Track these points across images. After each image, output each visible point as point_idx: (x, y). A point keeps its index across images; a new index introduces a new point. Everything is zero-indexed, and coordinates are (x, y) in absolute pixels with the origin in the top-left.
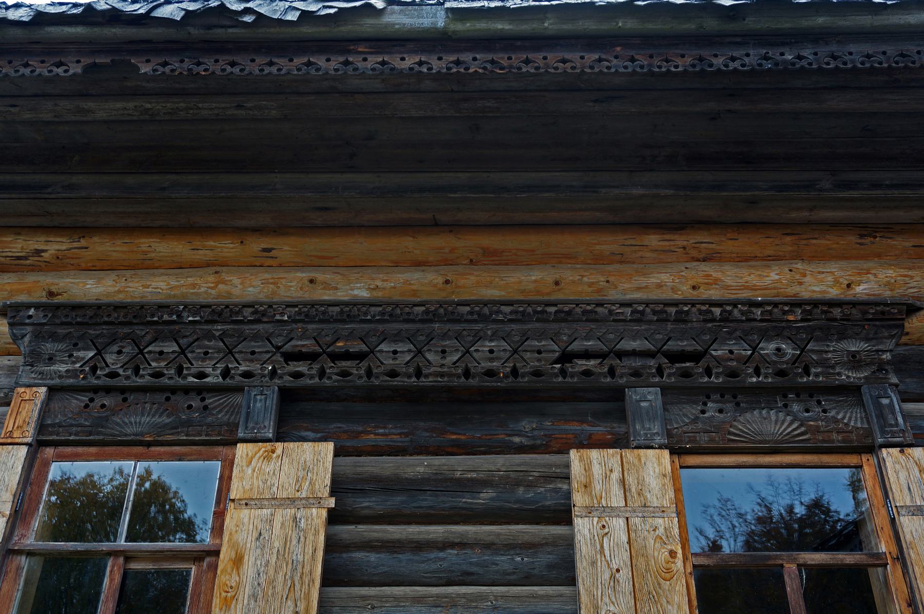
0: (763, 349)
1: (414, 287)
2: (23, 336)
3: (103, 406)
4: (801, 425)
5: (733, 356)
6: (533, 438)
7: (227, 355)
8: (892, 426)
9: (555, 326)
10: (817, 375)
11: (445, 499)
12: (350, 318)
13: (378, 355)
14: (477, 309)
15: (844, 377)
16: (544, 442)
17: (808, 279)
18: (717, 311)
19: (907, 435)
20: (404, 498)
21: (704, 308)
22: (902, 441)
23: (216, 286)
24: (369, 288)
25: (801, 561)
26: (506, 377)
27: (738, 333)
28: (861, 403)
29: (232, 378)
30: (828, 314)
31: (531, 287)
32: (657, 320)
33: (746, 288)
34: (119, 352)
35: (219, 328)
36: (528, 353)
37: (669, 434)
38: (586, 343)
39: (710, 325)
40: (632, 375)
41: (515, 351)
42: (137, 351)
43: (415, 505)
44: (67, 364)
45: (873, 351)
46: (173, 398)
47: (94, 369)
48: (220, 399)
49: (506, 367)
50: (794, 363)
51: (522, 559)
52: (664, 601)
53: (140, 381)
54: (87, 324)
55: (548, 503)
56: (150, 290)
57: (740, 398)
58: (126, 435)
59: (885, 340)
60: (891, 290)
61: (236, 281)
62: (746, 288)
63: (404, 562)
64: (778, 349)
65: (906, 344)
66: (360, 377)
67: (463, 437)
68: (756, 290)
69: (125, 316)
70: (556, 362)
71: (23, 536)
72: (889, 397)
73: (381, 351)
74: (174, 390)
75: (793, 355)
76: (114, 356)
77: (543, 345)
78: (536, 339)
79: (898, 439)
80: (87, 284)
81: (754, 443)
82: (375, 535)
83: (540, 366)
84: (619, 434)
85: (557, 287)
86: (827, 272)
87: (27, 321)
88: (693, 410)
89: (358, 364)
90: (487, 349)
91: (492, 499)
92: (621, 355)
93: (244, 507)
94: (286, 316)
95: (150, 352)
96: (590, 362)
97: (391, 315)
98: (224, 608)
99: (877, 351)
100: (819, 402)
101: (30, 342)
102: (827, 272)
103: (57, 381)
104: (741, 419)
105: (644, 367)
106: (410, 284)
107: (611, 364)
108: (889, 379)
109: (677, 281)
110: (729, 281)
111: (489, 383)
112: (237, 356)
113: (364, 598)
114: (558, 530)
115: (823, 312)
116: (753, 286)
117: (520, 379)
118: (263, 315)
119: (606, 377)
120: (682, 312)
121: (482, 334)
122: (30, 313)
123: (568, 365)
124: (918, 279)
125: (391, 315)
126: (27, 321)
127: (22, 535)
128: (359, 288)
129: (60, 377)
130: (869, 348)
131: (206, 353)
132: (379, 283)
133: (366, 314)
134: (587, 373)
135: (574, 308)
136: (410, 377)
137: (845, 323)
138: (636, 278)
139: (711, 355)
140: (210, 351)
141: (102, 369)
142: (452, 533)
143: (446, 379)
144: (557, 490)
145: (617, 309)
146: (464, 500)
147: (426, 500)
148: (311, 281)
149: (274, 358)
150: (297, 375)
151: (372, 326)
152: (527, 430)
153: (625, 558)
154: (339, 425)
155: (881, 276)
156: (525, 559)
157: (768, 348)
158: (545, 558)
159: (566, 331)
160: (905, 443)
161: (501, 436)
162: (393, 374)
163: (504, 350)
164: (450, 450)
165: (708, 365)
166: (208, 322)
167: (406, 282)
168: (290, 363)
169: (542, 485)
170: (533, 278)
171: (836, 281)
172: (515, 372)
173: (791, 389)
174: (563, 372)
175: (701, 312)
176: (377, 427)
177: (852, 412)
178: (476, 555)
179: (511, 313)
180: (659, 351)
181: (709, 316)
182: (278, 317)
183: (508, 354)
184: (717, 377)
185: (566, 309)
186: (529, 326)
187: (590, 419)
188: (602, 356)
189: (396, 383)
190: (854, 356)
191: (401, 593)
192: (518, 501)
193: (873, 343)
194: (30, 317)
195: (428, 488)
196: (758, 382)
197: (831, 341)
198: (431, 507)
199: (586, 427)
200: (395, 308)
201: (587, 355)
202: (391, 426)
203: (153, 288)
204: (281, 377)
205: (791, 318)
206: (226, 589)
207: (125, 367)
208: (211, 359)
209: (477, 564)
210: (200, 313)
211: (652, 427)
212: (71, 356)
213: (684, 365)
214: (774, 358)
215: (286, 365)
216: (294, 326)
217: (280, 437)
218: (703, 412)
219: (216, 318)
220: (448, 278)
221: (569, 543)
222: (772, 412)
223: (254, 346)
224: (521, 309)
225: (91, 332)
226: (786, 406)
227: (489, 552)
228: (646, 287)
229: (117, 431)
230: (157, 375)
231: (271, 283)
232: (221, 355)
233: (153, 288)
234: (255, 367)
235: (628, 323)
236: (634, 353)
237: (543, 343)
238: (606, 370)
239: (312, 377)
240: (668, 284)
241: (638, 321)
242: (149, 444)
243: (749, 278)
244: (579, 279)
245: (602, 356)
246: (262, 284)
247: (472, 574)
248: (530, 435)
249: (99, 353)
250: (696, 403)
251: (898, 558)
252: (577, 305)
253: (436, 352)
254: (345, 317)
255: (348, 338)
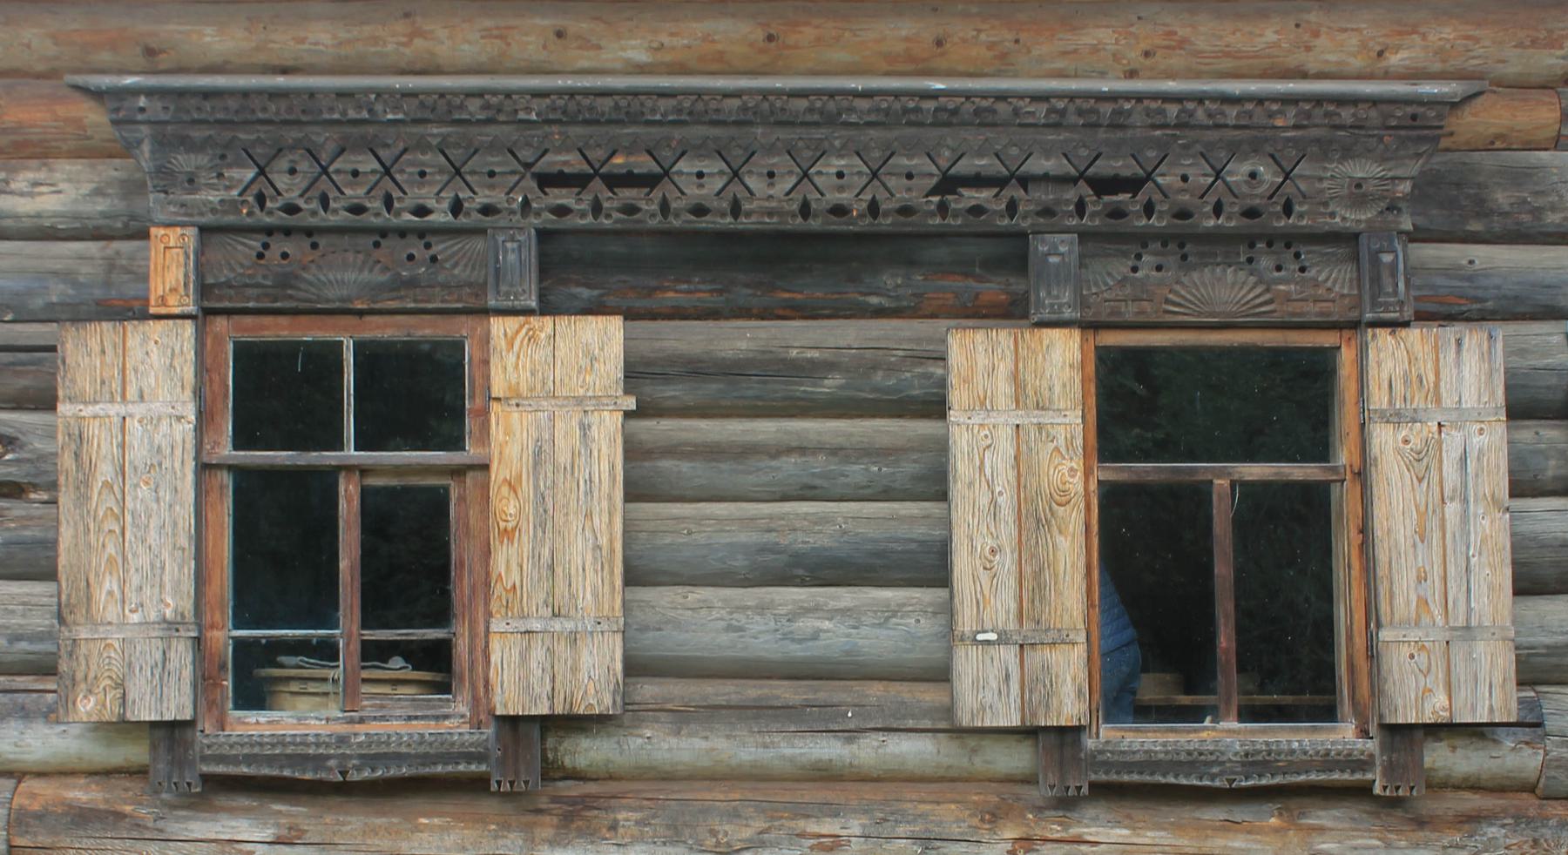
0: (1230, 173)
1: (719, 47)
2: (139, 142)
3: (285, 256)
4: (1267, 290)
5: (1185, 186)
6: (897, 298)
7: (453, 177)
8: (1388, 294)
9: (935, 133)
10: (1301, 216)
11: (777, 387)
12: (634, 118)
13: (676, 178)
14: (818, 104)
15: (1338, 220)
16: (912, 304)
17: (1322, 42)
18: (1173, 110)
19: (1406, 309)
20: (721, 386)
21: (1154, 105)
22: (1397, 318)
23: (411, 41)
24: (651, 48)
25: (1236, 477)
26: (861, 216)
27: (1199, 148)
28: (1356, 258)
29: (468, 214)
30: (1335, 118)
31: (900, 47)
32: (1083, 125)
33: (1227, 55)
34: (292, 171)
35: (435, 131)
36: (894, 178)
37: (1083, 303)
38: (977, 162)
39: (1158, 133)
40: (1039, 214)
41: (875, 175)
42: (319, 169)
43: (735, 394)
44: (218, 190)
45: (1387, 179)
46: (384, 242)
47: (261, 199)
48: (453, 246)
49: (861, 200)
50: (1271, 197)
51: (880, 469)
52: (1055, 529)
53: (333, 219)
54: (232, 122)
55: (916, 392)
56: (306, 46)
57: (1188, 248)
58: (328, 301)
59: (1407, 161)
60: (1444, 61)
61: (442, 33)
62: (1227, 55)
63: (724, 474)
64: (1253, 175)
65: (1447, 150)
66: (653, 215)
67: (799, 296)
68: (1241, 58)
69: (290, 110)
70: (932, 192)
71: (217, 444)
72: (1394, 251)
73: (680, 173)
74: (384, 233)
75: (1273, 183)
76: (286, 178)
77: (916, 165)
78: (905, 155)
79: (1392, 315)
80: (205, 35)
81: (1198, 316)
82: (684, 436)
83: (909, 200)
84: (1017, 294)
85: (939, 51)
86: (1353, 30)
87: (140, 117)
88: (1121, 267)
89: (648, 194)
90: (834, 170)
91: (840, 387)
92: (1025, 181)
93: (515, 408)
94: (534, 114)
95: (338, 171)
96: (981, 193)
97: (690, 113)
98: (505, 540)
99: (1393, 179)
100: (1297, 255)
101: (152, 152)
102: (1353, 30)
103: (209, 219)
104: (1185, 280)
105: (1058, 202)
106: (713, 41)
107: (1012, 197)
108: (1400, 223)
109: (1123, 42)
110: (1201, 44)
111: (837, 225)
112: (468, 178)
113: (678, 519)
114: (923, 428)
115: (1327, 114)
116: (1236, 52)
117: (881, 220)
118: (499, 111)
119: (1003, 216)
120: (1119, 112)
121: (826, 144)
122: (141, 104)
123: (950, 197)
124: (1487, 43)
125: (690, 113)
126: (140, 117)
127: (214, 442)
128: (633, 48)
129: (213, 211)
130: (1383, 173)
131: (422, 174)
132: (666, 40)
133: (654, 111)
134: (977, 210)
135: (962, 103)
136: (723, 215)
137: (1356, 131)
138: (1061, 36)
139: (1155, 182)
140: (428, 170)
141: (273, 199)
142: (787, 432)
143: (775, 220)
144: (928, 376)
145: (1026, 106)
146: (802, 388)
147: (751, 388)
148: (560, 34)
149: (523, 183)
150: (562, 211)
151: (665, 131)
152: (889, 287)
153: (1010, 478)
154: (623, 277)
155: (1432, 38)
156: (884, 469)
157: (1238, 172)
158: (908, 468)
159: (949, 141)
160: (1401, 320)
161: (851, 296)
162: (700, 210)
163: (859, 173)
164: (781, 312)
165: (1150, 199)
166: (416, 122)
167: (707, 38)
168: (547, 190)
169: (908, 369)
170: (904, 33)
171: (1364, 46)
172: (873, 209)
173: (1260, 237)
174: (943, 209)
175: (1148, 112)
176: (678, 281)
177: (1340, 271)
178: (819, 463)
179: (870, 111)
180: (1082, 175)
181: (1158, 120)
182: (522, 115)
183: (865, 180)
184: (1160, 218)
185: (951, 106)
186: (896, 133)
187: (977, 270)
188: (999, 182)
189: (704, 225)
190: (1359, 186)
191: (725, 513)
192: (875, 389)
193: (1388, 167)
194: (142, 110)
195: (753, 373)
196: (1217, 227)
197: (1332, 161)
198: (758, 398)
199: (971, 283)
200: (697, 100)
201: (978, 181)
202: (697, 279)
203: (311, 44)
204: (538, 214)
205: (1279, 122)
206: (504, 517)
207: (306, 196)
208: (431, 184)
209: (821, 476)
210: (402, 106)
211: (1061, 295)
212: (220, 175)
213: (1115, 198)
214: (1245, 189)
215: (542, 195)
216: (547, 128)
217: (547, 308)
218: (1135, 270)
219: (428, 115)
220: (772, 32)
221: (942, 447)
222: (1230, 270)
223: (493, 163)
224: (884, 105)
225: (242, 136)
226: (1250, 260)
227: (836, 459)
228: (1075, 51)
229: (314, 294)
230: (357, 210)
231: (496, 37)
232: (445, 178)
233: (311, 44)
234: (496, 197)
235: (1041, 129)
236: (1046, 178)
237: (915, 162)
238: (1003, 206)
239: (583, 215)
240: (1108, 47)
241: (1056, 126)
242: (361, 313)
243: (1230, 39)
244: (973, 37)
245: (999, 182)
246: (482, 37)
247: (815, 488)
248: (892, 294)
249: (262, 172)
250: (1125, 255)
251: (1359, 473)
252: (968, 98)
253: (760, 175)
254: (622, 116)
255: (630, 151)
